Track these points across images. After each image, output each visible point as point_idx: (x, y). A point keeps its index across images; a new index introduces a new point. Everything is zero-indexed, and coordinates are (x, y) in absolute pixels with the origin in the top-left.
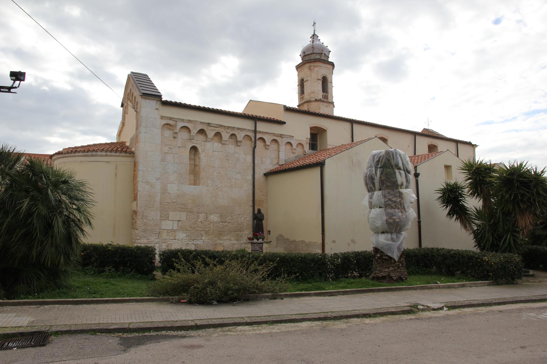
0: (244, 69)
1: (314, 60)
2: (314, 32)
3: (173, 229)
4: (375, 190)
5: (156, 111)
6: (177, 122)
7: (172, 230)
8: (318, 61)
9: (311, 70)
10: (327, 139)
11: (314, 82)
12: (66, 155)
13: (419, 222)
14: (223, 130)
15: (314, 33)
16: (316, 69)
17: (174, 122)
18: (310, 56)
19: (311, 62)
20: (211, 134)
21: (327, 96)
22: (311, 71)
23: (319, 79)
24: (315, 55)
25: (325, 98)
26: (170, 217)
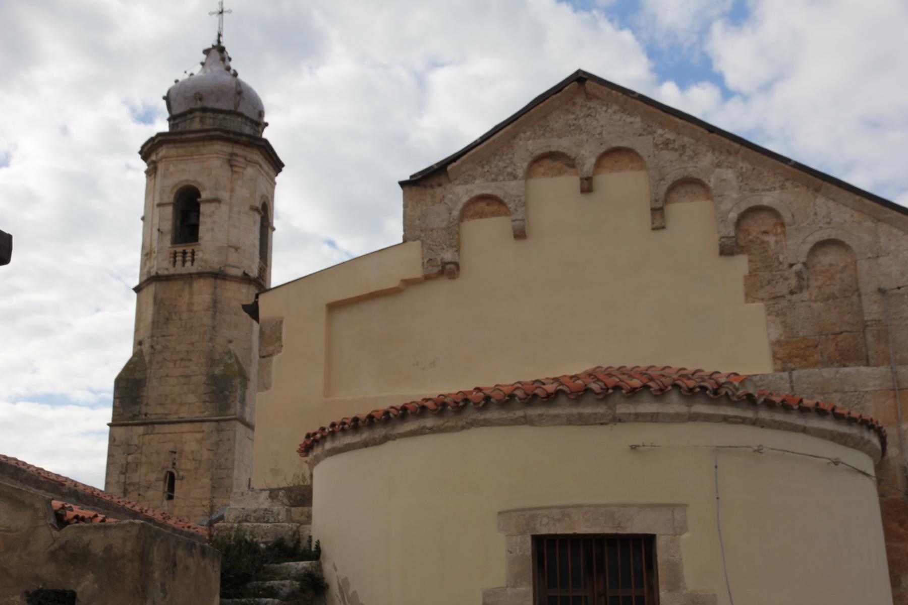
9: (236, 169)
15: (219, 42)
16: (250, 171)
18: (224, 119)
22: (236, 172)
24: (239, 119)
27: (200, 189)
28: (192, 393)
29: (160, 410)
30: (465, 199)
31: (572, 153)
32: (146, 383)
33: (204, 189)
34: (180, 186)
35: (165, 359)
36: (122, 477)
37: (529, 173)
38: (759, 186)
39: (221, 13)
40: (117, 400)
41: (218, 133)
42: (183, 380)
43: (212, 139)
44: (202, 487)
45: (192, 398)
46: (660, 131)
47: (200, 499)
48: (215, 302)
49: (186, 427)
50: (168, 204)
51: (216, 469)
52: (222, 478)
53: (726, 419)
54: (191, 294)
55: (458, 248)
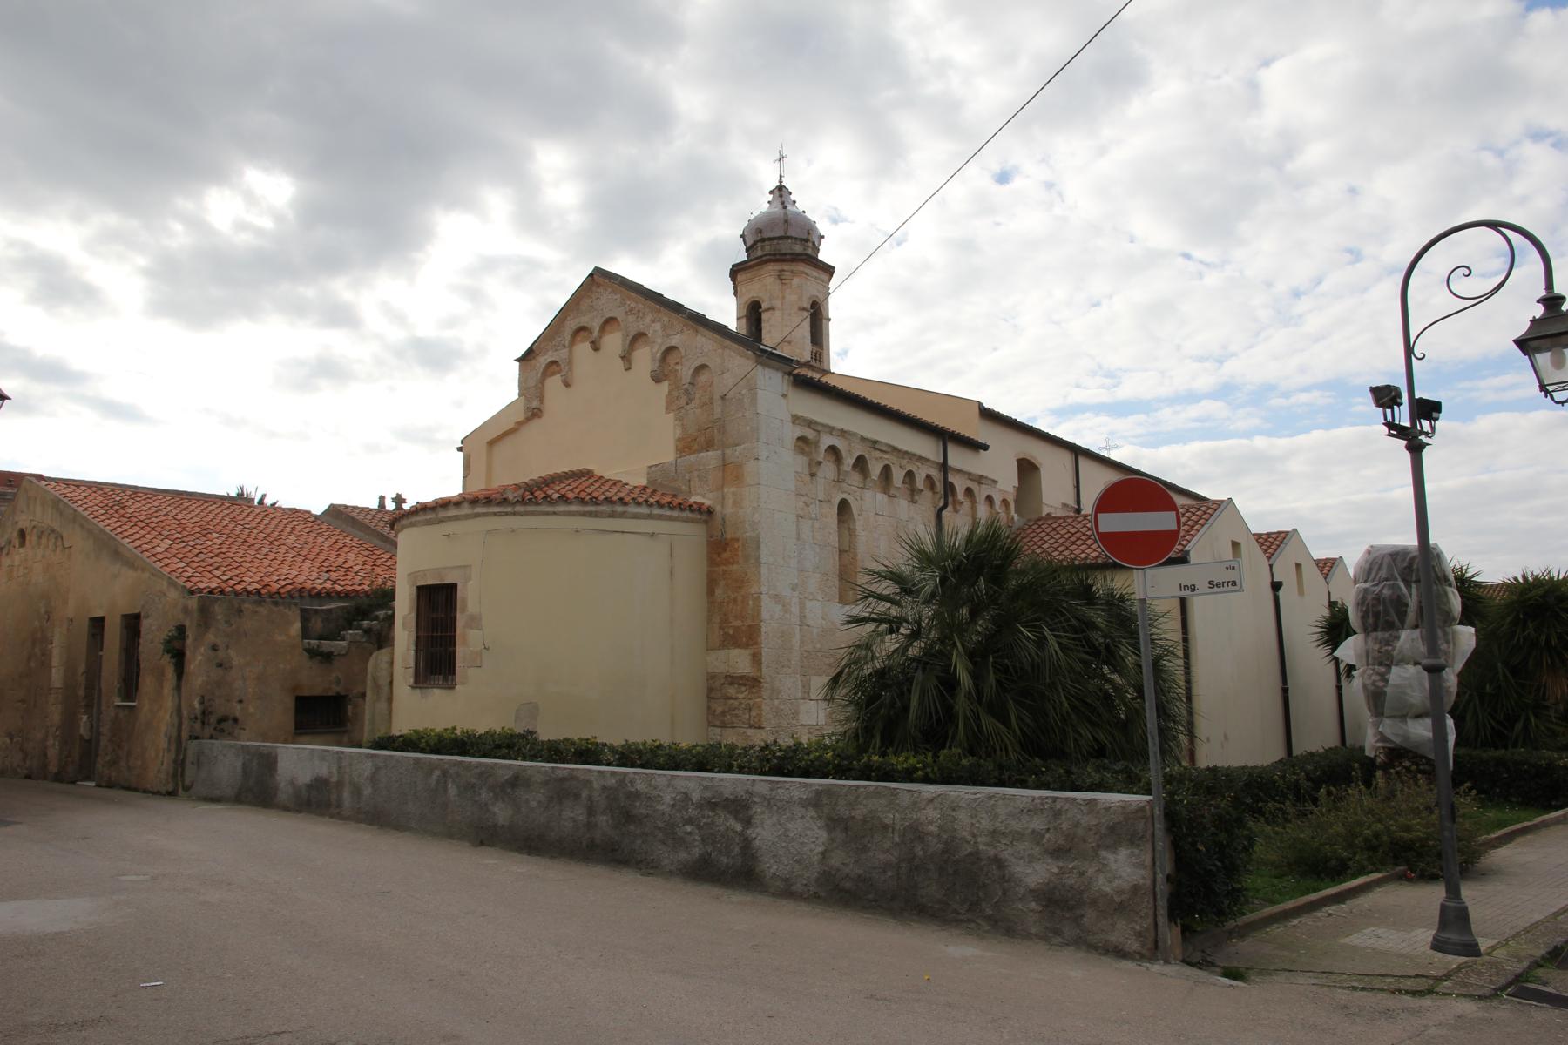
0: (311, 213)
1: (794, 257)
2: (781, 179)
3: (817, 725)
4: (1403, 628)
5: (783, 401)
6: (819, 434)
7: (817, 727)
8: (803, 261)
9: (784, 281)
10: (1041, 489)
11: (790, 314)
12: (519, 508)
13: (1285, 691)
14: (895, 459)
15: (781, 182)
16: (796, 281)
17: (815, 434)
18: (778, 244)
19: (784, 261)
20: (875, 469)
21: (820, 355)
22: (785, 284)
23: (804, 309)
24: (790, 241)
25: (816, 359)
26: (812, 690)
30: (544, 365)
34: (749, 302)
38: (672, 333)
41: (768, 257)
43: (767, 262)
46: (629, 303)
50: (742, 317)
53: (495, 514)
55: (541, 400)
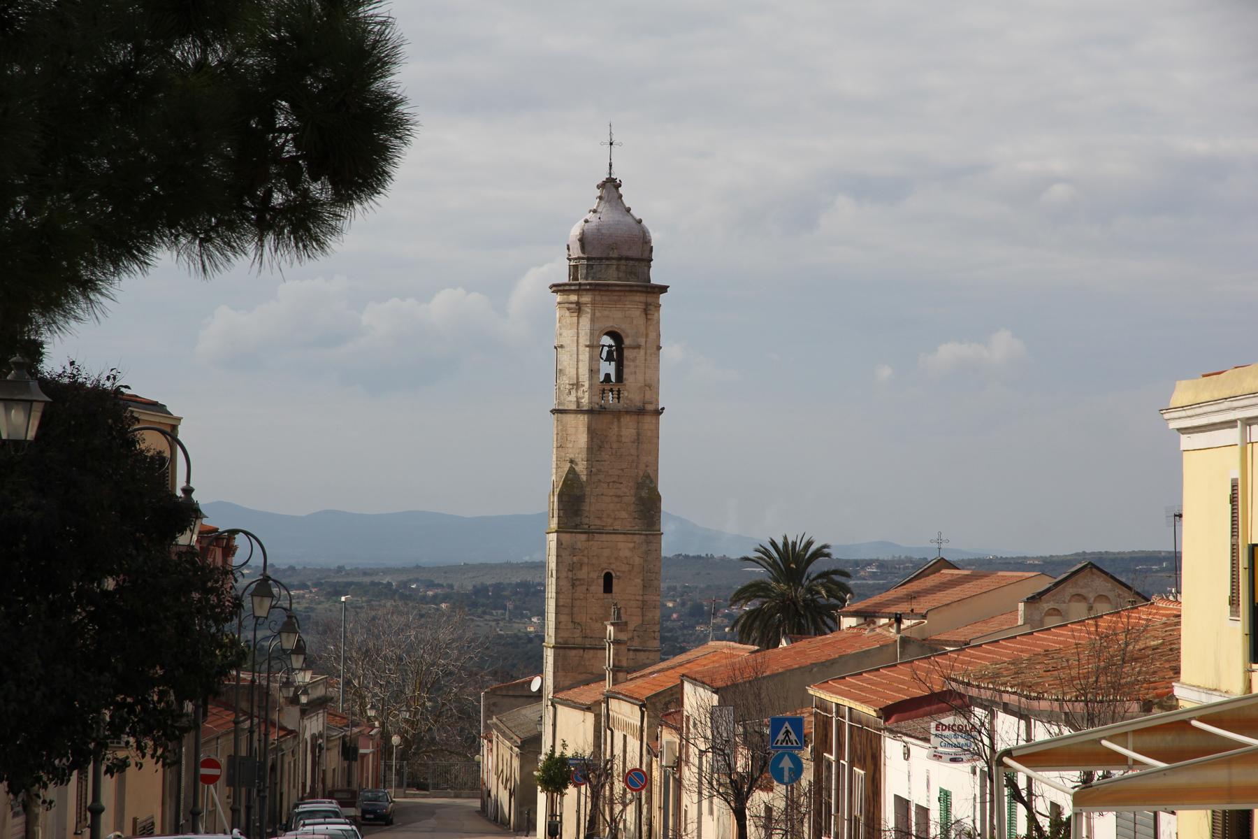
27: (623, 335)
28: (624, 510)
29: (598, 522)
30: (1047, 609)
31: (1086, 595)
32: (584, 499)
33: (627, 336)
35: (600, 481)
36: (570, 573)
37: (1070, 601)
39: (611, 144)
40: (561, 512)
42: (616, 500)
44: (635, 586)
45: (624, 515)
46: (1117, 590)
47: (635, 595)
48: (638, 434)
49: (621, 537)
51: (647, 572)
52: (652, 580)
54: (619, 427)
